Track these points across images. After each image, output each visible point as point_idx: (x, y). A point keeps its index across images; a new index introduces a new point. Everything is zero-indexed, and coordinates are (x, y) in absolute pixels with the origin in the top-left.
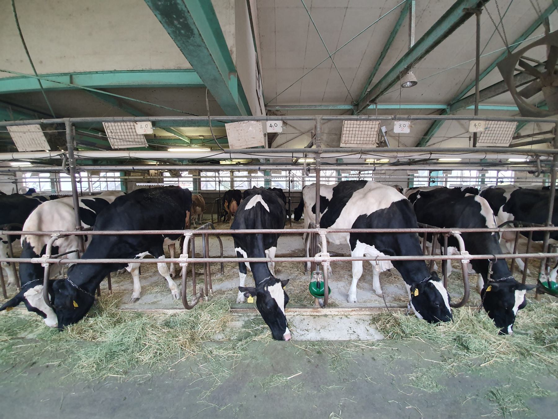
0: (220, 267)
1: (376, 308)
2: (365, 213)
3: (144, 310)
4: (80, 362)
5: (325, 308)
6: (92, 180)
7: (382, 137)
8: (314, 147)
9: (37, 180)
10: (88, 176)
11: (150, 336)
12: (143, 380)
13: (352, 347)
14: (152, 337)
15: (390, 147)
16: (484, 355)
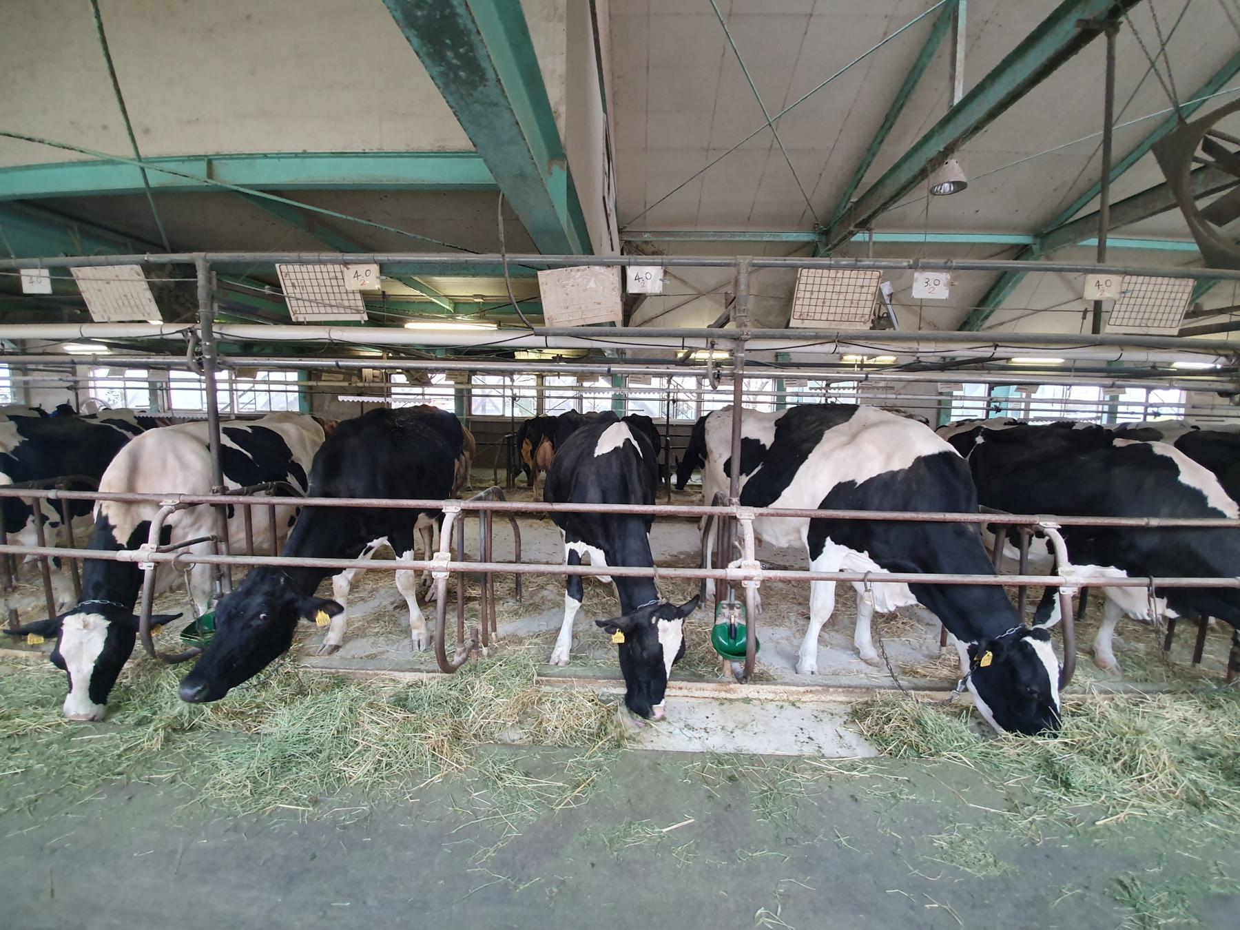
0: (513, 585)
1: (861, 688)
2: (851, 479)
3: (351, 671)
4: (216, 775)
5: (746, 682)
6: (239, 388)
7: (882, 306)
8: (730, 327)
9: (121, 384)
10: (230, 378)
11: (367, 726)
12: (350, 819)
13: (806, 770)
14: (371, 728)
15: (899, 329)
16: (1103, 802)
